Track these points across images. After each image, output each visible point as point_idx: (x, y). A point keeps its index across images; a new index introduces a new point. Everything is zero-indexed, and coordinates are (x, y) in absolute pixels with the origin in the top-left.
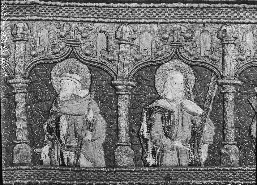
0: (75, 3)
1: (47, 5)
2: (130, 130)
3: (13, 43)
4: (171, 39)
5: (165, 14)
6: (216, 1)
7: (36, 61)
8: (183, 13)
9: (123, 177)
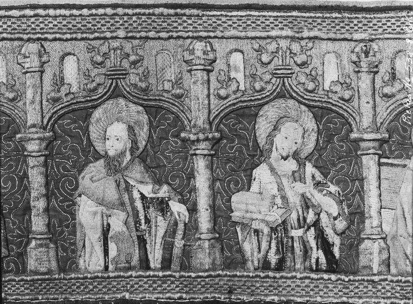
0: (173, 10)
1: (41, 16)
2: (213, 207)
3: (355, 75)
6: (258, 4)
9: (204, 285)
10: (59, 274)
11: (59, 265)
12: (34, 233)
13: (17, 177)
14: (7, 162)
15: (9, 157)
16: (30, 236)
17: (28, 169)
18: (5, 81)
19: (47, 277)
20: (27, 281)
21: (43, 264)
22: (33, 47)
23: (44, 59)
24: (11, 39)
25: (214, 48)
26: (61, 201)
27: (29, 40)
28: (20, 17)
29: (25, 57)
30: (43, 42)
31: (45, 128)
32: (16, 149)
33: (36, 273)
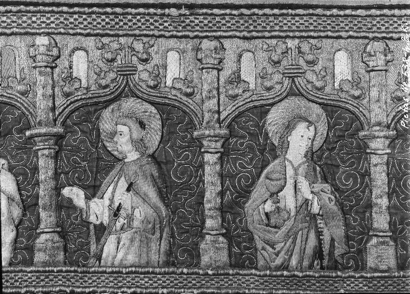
4: (284, 63)
5: (339, 25)
10: (399, 273)
11: (397, 263)
12: (375, 230)
13: (359, 174)
14: (349, 159)
15: (351, 154)
16: (371, 233)
17: (370, 167)
18: (350, 79)
19: (387, 274)
20: (367, 278)
21: (384, 262)
22: (379, 46)
23: (389, 57)
24: (357, 38)
25: (225, 47)
26: (403, 199)
27: (374, 39)
28: (366, 16)
29: (371, 55)
30: (387, 41)
31: (388, 127)
32: (359, 147)
33: (376, 270)
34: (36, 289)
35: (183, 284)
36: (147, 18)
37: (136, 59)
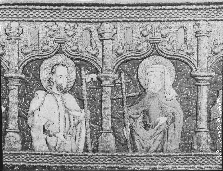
0: (38, 6)
4: (56, 35)
7: (120, 61)
8: (71, 14)
34: (20, 163)
35: (59, 159)
36: (120, 12)
37: (66, 35)
